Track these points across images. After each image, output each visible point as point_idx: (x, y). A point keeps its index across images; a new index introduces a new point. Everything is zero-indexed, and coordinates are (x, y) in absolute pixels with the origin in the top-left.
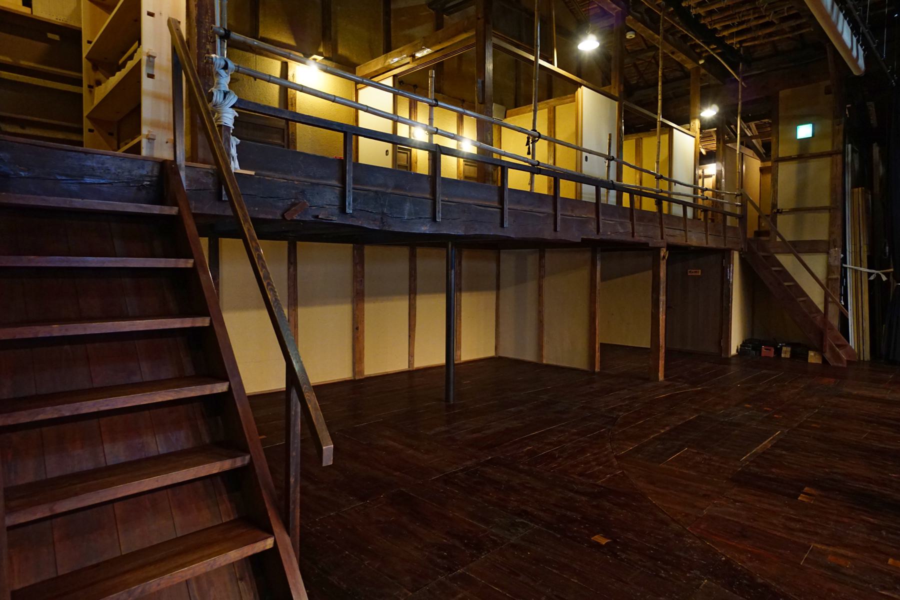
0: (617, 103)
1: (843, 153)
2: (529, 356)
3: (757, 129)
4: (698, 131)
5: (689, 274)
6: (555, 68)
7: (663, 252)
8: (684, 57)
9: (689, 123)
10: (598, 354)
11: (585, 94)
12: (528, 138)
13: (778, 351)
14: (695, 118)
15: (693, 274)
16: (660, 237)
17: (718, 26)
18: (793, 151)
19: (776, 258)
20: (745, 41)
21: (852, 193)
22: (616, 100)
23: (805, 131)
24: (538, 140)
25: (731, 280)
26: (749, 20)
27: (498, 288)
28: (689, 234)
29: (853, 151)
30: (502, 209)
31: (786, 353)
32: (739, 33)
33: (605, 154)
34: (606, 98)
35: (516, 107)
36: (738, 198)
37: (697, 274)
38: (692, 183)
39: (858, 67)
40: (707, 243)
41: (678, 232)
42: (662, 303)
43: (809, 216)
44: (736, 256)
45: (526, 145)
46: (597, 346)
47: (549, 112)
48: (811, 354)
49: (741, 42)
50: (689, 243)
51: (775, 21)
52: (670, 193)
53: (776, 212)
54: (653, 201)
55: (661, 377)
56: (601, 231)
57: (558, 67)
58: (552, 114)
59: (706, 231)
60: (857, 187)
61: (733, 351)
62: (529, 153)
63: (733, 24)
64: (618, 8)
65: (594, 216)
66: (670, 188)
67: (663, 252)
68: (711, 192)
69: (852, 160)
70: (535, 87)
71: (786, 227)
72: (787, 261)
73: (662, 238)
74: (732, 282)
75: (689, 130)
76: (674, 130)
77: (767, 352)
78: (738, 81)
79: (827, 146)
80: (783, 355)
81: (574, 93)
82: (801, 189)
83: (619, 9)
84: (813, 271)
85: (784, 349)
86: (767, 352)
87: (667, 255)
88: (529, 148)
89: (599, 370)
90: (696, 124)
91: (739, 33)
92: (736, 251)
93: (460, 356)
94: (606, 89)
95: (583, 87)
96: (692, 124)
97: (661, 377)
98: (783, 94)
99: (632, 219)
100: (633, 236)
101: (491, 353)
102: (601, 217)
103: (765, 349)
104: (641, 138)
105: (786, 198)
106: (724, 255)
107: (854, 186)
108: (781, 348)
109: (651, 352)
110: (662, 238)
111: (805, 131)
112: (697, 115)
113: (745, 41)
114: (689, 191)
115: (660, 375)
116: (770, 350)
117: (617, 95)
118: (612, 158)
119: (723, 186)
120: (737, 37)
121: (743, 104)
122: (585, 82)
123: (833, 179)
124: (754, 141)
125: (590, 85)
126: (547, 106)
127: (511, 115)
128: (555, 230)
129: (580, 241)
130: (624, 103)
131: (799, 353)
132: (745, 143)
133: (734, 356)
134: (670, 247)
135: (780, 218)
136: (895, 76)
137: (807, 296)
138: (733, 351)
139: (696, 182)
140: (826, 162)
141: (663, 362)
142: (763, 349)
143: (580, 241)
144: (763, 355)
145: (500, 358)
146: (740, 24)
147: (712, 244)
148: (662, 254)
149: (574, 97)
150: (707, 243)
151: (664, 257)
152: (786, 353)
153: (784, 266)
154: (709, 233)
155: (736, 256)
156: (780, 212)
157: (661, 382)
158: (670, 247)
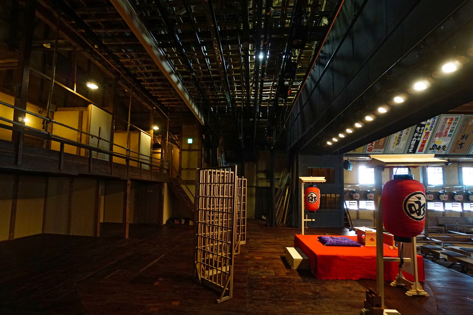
0: (111, 115)
1: (201, 151)
2: (63, 232)
3: (178, 138)
4: (152, 134)
5: (148, 192)
6: (75, 92)
7: (129, 182)
8: (147, 104)
9: (149, 130)
10: (99, 228)
11: (93, 108)
12: (44, 121)
13: (181, 221)
14: (151, 129)
15: (150, 192)
16: (127, 176)
17: (159, 96)
18: (187, 148)
19: (181, 186)
20: (171, 104)
21: (204, 164)
22: (111, 114)
23: (190, 141)
24: (49, 123)
25: (163, 194)
26: (169, 97)
27: (46, 197)
28: (142, 175)
29: (204, 150)
30: (17, 155)
31: (183, 222)
32: (167, 101)
33: (97, 136)
34: (106, 112)
35: (65, 107)
36: (167, 162)
37: (151, 192)
38: (149, 156)
39: (202, 123)
40: (151, 179)
41: (137, 174)
42: (127, 204)
43: (191, 171)
44: (166, 185)
45: (43, 124)
46: (98, 225)
47: (80, 113)
48: (190, 222)
49: (169, 104)
50: (142, 178)
51: (179, 100)
52: (139, 158)
53: (181, 169)
54: (125, 160)
55: (127, 237)
56: (91, 171)
57: (76, 92)
58: (81, 114)
59: (151, 174)
60: (205, 163)
61: (164, 222)
62: (43, 128)
63: (165, 97)
64: (114, 76)
65: (88, 164)
66: (139, 156)
67: (129, 182)
68: (160, 160)
69: (204, 153)
70: (50, 97)
71: (184, 177)
72: (183, 187)
73: (128, 176)
74: (164, 195)
75: (149, 133)
76: (141, 132)
77: (177, 222)
78: (168, 118)
79: (196, 147)
80: (182, 223)
81: (87, 107)
82: (189, 161)
83: (114, 76)
84: (192, 192)
85: (183, 220)
86: (177, 222)
87: (130, 184)
88: (44, 126)
89: (99, 236)
90: (152, 131)
91: (167, 101)
92: (165, 183)
93: (14, 235)
94: (106, 108)
95: (92, 104)
96: (150, 131)
97: (127, 237)
98: (184, 126)
99: (111, 167)
100: (111, 174)
101: (40, 232)
102: (91, 164)
103: (176, 221)
104: (130, 133)
105: (184, 165)
106: (161, 184)
107: (204, 162)
108: (181, 221)
109: (123, 226)
110: (128, 176)
111: (190, 141)
112: (152, 128)
113: (171, 104)
114: (148, 158)
115: (126, 236)
116: (177, 221)
117: (112, 112)
118: (100, 138)
119: (164, 157)
120: (166, 102)
121: (169, 127)
122: (93, 103)
123: (198, 159)
124: (176, 142)
125: (95, 103)
126: (79, 110)
127: (59, 111)
128: (60, 168)
129: (77, 175)
130: (115, 116)
131: (187, 222)
132: (173, 142)
133: (165, 224)
134: (132, 180)
135: (182, 171)
136: (329, 143)
137: (191, 200)
138: (164, 222)
139: (151, 154)
140: (196, 152)
141: (128, 230)
142: (175, 221)
143: (77, 175)
144: (175, 223)
145: (45, 234)
146: (167, 97)
147: (154, 180)
148: (128, 183)
149: (87, 109)
150: (151, 179)
151: (129, 184)
152: (183, 222)
153: (184, 189)
154: (152, 175)
155: (166, 185)
156: (182, 169)
157: (127, 239)
158: (132, 180)
